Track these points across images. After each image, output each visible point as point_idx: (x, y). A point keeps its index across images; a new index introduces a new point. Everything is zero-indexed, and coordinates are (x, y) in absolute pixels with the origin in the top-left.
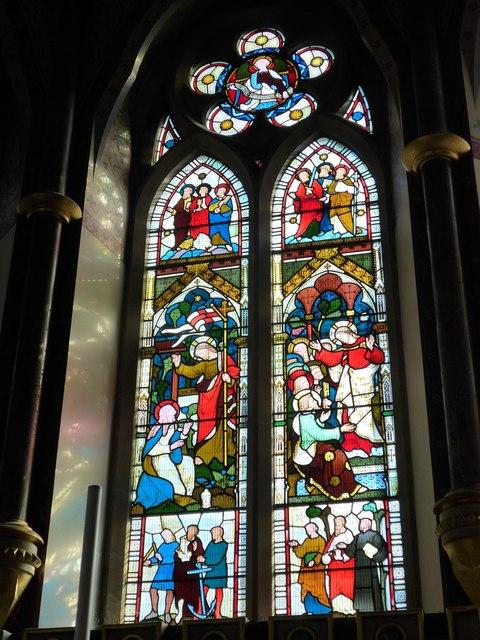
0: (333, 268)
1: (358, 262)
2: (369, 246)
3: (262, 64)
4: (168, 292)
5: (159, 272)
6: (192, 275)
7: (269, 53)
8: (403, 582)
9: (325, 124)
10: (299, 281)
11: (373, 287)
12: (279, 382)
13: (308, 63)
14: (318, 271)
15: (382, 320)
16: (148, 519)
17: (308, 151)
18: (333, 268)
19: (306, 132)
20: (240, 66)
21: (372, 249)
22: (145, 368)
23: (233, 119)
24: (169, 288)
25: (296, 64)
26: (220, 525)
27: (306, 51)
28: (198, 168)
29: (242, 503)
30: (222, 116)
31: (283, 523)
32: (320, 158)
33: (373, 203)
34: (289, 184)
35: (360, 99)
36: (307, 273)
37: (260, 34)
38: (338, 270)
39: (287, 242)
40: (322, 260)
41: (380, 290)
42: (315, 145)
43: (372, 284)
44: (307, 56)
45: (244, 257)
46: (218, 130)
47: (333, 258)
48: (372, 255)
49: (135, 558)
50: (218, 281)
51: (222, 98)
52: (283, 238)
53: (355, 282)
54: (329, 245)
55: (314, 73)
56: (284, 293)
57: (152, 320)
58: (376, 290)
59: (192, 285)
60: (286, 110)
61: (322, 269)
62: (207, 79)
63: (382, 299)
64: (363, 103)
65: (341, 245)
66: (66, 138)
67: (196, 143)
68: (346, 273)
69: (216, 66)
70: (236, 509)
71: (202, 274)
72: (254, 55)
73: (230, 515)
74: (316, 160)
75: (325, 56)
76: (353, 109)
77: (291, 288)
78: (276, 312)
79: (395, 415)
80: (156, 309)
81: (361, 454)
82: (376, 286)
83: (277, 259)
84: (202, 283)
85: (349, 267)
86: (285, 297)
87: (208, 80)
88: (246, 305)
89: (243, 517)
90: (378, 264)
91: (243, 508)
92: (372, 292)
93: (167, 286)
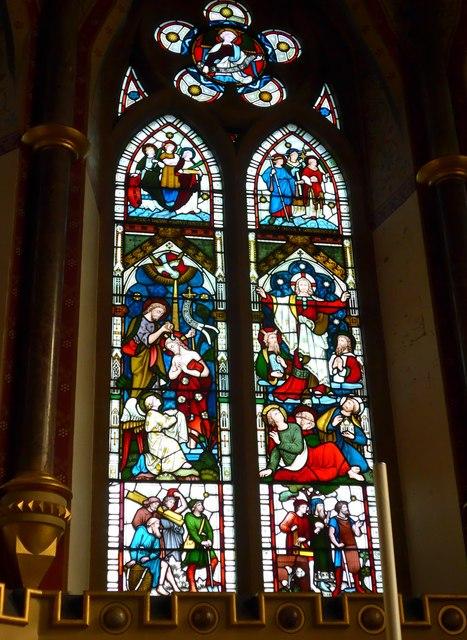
1: (330, 254)
3: (228, 37)
4: (138, 250)
6: (296, 247)
7: (235, 27)
9: (296, 113)
12: (222, 358)
13: (180, 43)
14: (291, 257)
15: (222, 307)
16: (126, 484)
19: (274, 119)
20: (207, 33)
21: (214, 236)
22: (117, 324)
23: (202, 86)
24: (140, 246)
25: (263, 45)
26: (213, 501)
27: (270, 33)
28: (165, 126)
29: (227, 477)
30: (189, 80)
32: (290, 143)
33: (218, 191)
34: (135, 154)
35: (326, 95)
37: (225, 5)
43: (213, 271)
44: (272, 38)
48: (214, 244)
55: (282, 58)
57: (122, 277)
58: (217, 279)
59: (295, 255)
60: (256, 90)
62: (173, 37)
63: (222, 288)
67: (164, 102)
69: (184, 25)
70: (221, 483)
72: (220, 26)
73: (213, 488)
74: (161, 137)
75: (291, 44)
76: (320, 104)
78: (116, 282)
79: (231, 402)
80: (261, 274)
82: (348, 282)
83: (119, 229)
84: (305, 256)
85: (322, 257)
86: (126, 269)
87: (173, 37)
88: (351, 286)
89: (228, 489)
90: (349, 261)
91: (227, 482)
93: (137, 243)
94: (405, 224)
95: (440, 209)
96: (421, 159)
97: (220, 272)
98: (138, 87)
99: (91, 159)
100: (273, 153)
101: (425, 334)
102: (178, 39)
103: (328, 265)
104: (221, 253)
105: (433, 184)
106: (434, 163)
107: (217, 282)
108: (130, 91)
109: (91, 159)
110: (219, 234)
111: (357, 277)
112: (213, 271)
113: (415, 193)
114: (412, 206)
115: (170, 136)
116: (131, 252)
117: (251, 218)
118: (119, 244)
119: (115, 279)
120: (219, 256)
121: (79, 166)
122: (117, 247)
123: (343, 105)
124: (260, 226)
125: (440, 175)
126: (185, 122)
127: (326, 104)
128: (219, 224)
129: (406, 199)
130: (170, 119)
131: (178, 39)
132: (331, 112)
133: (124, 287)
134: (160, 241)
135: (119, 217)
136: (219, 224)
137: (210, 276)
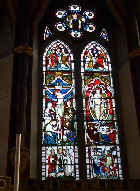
0: (99, 79)
2: (70, 73)
4: (50, 79)
5: (85, 74)
8: (121, 169)
9: (95, 37)
10: (89, 81)
11: (110, 86)
17: (90, 44)
18: (99, 79)
20: (81, 14)
21: (110, 75)
24: (50, 78)
31: (44, 169)
36: (91, 79)
38: (100, 79)
39: (86, 70)
40: (57, 75)
41: (112, 87)
42: (92, 43)
43: (110, 85)
45: (111, 73)
46: (57, 27)
47: (99, 76)
48: (110, 76)
49: (121, 170)
50: (65, 78)
51: (63, 20)
52: (84, 69)
53: (66, 83)
54: (60, 71)
56: (85, 84)
61: (95, 79)
62: (60, 14)
64: (49, 31)
65: (62, 71)
66: (137, 27)
67: (56, 35)
68: (102, 80)
71: (60, 75)
77: (87, 83)
78: (83, 89)
81: (56, 141)
82: (111, 86)
84: (60, 78)
86: (85, 85)
88: (112, 87)
92: (110, 87)
94: (126, 69)
95: (135, 63)
96: (17, 44)
97: (112, 85)
98: (49, 32)
99: (35, 54)
100: (52, 48)
101: (7, 96)
102: (61, 14)
103: (105, 81)
104: (74, 79)
105: (19, 53)
106: (21, 47)
107: (111, 88)
108: (47, 33)
109: (35, 54)
110: (73, 74)
111: (114, 83)
112: (110, 85)
113: (129, 60)
114: (128, 63)
115: (95, 47)
116: (48, 80)
117: (82, 69)
118: (44, 77)
119: (83, 88)
120: (111, 81)
121: (31, 57)
122: (44, 78)
123: (109, 35)
124: (47, 70)
125: (22, 51)
126: (98, 42)
127: (104, 34)
128: (110, 71)
129: (5, 57)
130: (94, 42)
131: (61, 14)
132: (106, 36)
133: (85, 90)
134: (94, 77)
135: (83, 71)
136: (110, 71)
137: (109, 86)
